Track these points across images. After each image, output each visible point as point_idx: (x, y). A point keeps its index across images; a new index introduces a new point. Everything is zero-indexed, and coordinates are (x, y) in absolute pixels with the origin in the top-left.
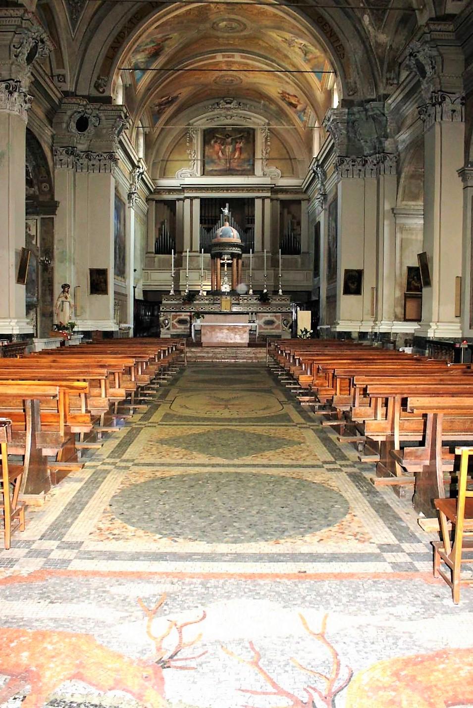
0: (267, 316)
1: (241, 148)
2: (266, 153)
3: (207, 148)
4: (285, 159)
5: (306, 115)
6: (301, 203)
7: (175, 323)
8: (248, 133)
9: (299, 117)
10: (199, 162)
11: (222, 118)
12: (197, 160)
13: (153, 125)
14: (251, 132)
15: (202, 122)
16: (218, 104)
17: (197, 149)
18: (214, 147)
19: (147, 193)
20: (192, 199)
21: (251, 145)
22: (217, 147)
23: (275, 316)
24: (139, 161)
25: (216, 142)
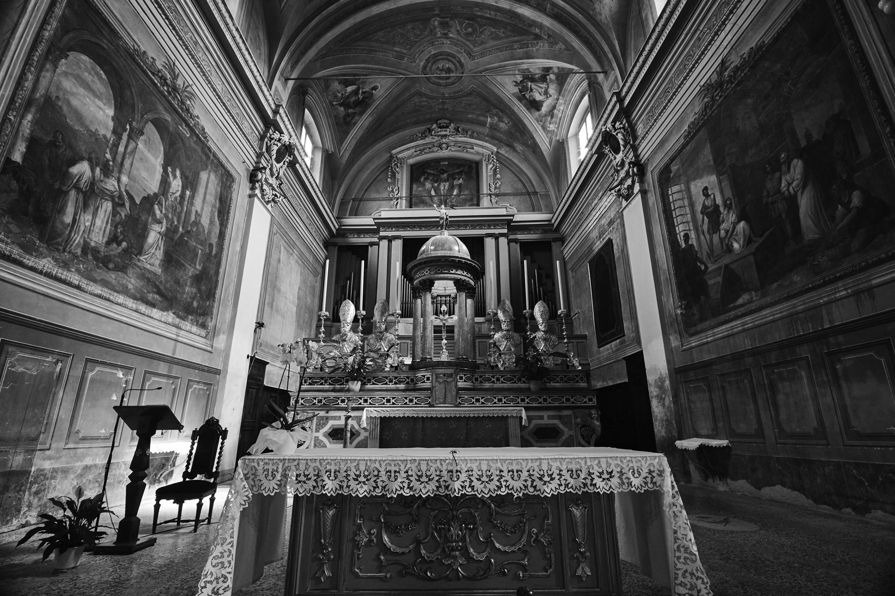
0: (542, 418)
1: (460, 186)
2: (496, 188)
3: (415, 186)
4: (521, 194)
5: (554, 119)
6: (550, 249)
7: (322, 438)
8: (470, 167)
9: (544, 128)
10: (404, 201)
11: (436, 149)
12: (401, 198)
13: (339, 141)
14: (474, 165)
15: (408, 154)
16: (430, 130)
17: (402, 185)
18: (424, 185)
19: (326, 233)
20: (390, 240)
21: (474, 182)
22: (428, 185)
23: (560, 418)
24: (276, 112)
25: (426, 179)
